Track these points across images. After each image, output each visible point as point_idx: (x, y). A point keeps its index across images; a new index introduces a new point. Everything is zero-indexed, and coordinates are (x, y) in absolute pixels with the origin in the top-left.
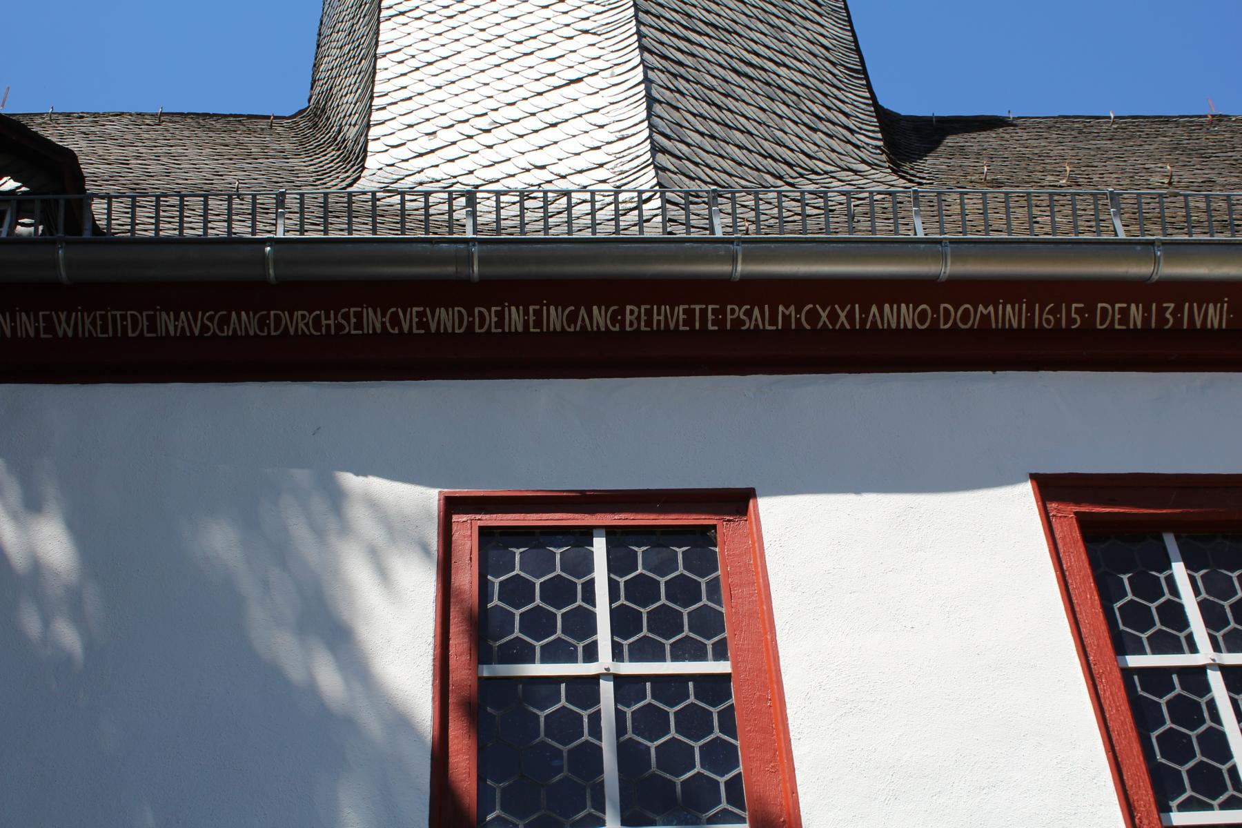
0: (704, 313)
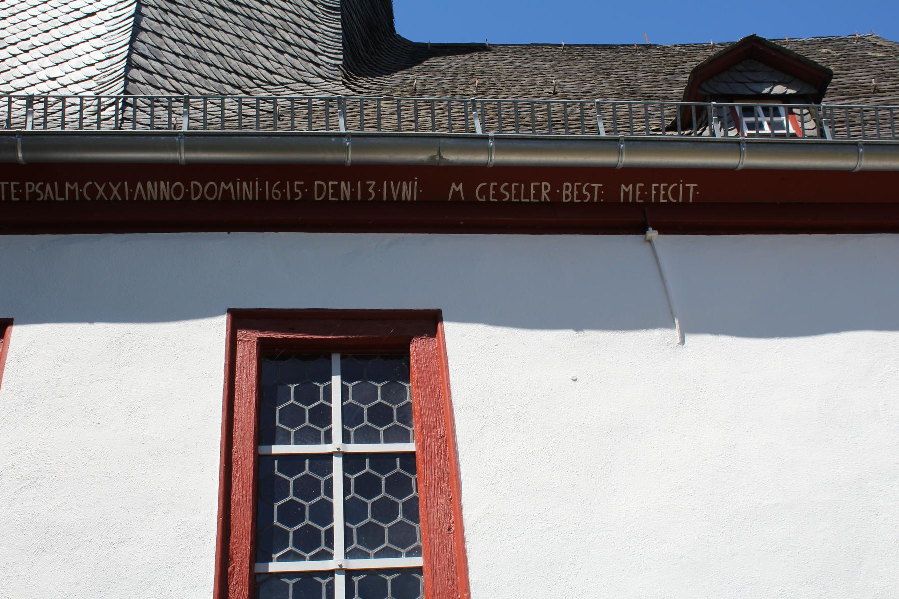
0: (8, 187)
